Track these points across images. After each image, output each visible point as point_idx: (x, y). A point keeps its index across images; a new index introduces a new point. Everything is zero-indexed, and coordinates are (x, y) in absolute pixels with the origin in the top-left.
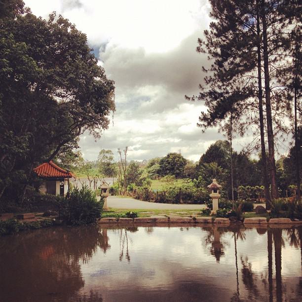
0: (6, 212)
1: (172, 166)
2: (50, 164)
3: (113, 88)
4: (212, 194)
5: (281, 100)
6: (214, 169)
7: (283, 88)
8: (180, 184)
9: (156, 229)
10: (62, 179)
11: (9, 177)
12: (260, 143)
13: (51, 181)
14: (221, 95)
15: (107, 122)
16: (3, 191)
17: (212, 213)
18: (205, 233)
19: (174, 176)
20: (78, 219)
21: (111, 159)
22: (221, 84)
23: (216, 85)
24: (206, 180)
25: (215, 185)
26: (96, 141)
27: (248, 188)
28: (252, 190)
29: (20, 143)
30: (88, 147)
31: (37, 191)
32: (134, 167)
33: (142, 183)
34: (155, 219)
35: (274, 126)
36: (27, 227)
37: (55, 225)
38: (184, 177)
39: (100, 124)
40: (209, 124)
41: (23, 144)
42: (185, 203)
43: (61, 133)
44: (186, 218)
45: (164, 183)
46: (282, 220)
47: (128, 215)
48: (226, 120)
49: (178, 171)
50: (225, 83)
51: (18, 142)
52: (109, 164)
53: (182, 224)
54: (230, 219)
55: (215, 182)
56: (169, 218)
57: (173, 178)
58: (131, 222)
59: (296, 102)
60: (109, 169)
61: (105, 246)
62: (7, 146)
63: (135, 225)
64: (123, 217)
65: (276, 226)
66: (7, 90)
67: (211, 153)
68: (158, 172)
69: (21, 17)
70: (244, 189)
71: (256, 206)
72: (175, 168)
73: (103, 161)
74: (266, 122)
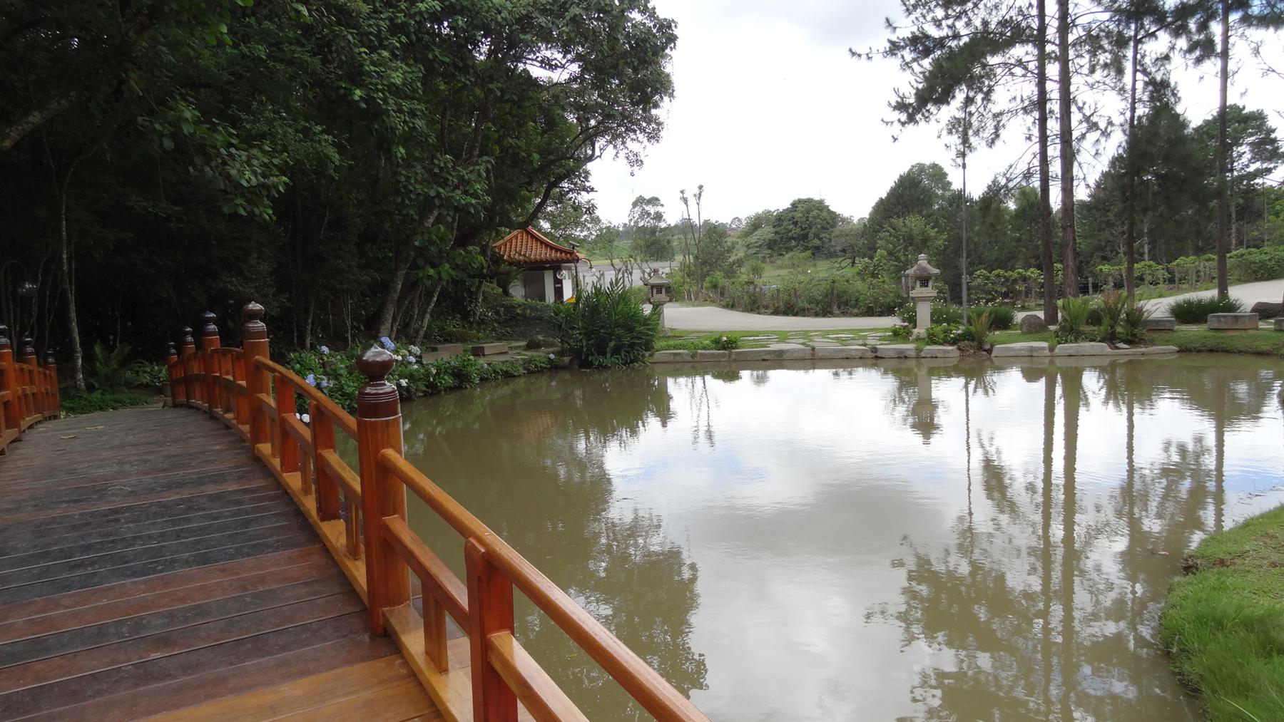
0: (446, 341)
1: (803, 228)
2: (528, 233)
3: (672, 39)
4: (918, 291)
5: (1101, 47)
6: (916, 231)
7: (1107, 16)
8: (821, 272)
9: (776, 375)
10: (556, 266)
11: (448, 262)
12: (1036, 162)
13: (534, 270)
14: (940, 43)
15: (659, 124)
16: (436, 295)
17: (914, 337)
18: (890, 383)
19: (808, 253)
20: (604, 354)
21: (659, 216)
22: (940, 13)
23: (929, 18)
24: (897, 259)
25: (924, 269)
26: (632, 174)
27: (998, 276)
28: (1007, 279)
29: (468, 182)
30: (615, 185)
31: (506, 293)
32: (714, 232)
33: (734, 272)
34: (781, 353)
35: (1076, 117)
36: (495, 371)
37: (554, 367)
38: (831, 255)
39: (643, 130)
40: (911, 119)
41: (475, 184)
42: (844, 314)
43: (552, 157)
44: (855, 347)
45: (784, 272)
46: (1087, 346)
47: (717, 343)
48: (952, 109)
49: (817, 242)
50: (950, 12)
51: (463, 182)
52: (653, 230)
53: (845, 362)
54: (959, 349)
55: (922, 260)
56: (813, 349)
57: (807, 259)
58: (725, 358)
59: (1136, 52)
60: (654, 243)
61: (665, 415)
62: (441, 190)
63: (734, 365)
64: (704, 348)
65: (1073, 363)
66: (430, 56)
67: (901, 196)
68: (771, 245)
69: (1193, 15)
70: (988, 278)
71: (1019, 316)
72: (811, 235)
73: (641, 224)
74: (1053, 114)
